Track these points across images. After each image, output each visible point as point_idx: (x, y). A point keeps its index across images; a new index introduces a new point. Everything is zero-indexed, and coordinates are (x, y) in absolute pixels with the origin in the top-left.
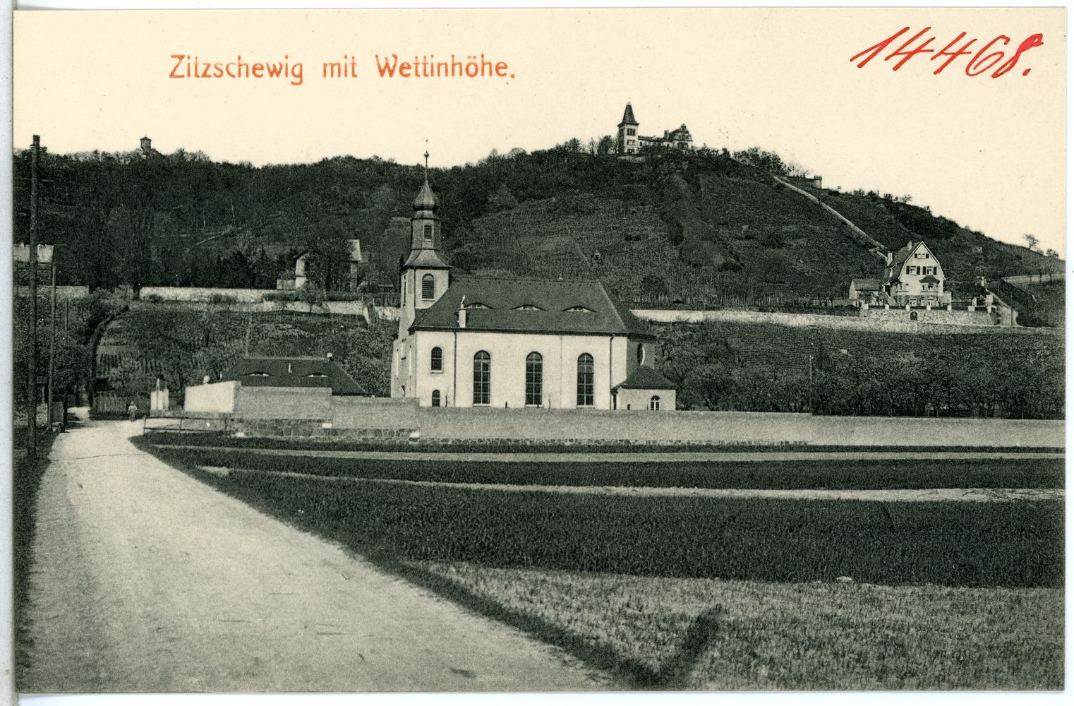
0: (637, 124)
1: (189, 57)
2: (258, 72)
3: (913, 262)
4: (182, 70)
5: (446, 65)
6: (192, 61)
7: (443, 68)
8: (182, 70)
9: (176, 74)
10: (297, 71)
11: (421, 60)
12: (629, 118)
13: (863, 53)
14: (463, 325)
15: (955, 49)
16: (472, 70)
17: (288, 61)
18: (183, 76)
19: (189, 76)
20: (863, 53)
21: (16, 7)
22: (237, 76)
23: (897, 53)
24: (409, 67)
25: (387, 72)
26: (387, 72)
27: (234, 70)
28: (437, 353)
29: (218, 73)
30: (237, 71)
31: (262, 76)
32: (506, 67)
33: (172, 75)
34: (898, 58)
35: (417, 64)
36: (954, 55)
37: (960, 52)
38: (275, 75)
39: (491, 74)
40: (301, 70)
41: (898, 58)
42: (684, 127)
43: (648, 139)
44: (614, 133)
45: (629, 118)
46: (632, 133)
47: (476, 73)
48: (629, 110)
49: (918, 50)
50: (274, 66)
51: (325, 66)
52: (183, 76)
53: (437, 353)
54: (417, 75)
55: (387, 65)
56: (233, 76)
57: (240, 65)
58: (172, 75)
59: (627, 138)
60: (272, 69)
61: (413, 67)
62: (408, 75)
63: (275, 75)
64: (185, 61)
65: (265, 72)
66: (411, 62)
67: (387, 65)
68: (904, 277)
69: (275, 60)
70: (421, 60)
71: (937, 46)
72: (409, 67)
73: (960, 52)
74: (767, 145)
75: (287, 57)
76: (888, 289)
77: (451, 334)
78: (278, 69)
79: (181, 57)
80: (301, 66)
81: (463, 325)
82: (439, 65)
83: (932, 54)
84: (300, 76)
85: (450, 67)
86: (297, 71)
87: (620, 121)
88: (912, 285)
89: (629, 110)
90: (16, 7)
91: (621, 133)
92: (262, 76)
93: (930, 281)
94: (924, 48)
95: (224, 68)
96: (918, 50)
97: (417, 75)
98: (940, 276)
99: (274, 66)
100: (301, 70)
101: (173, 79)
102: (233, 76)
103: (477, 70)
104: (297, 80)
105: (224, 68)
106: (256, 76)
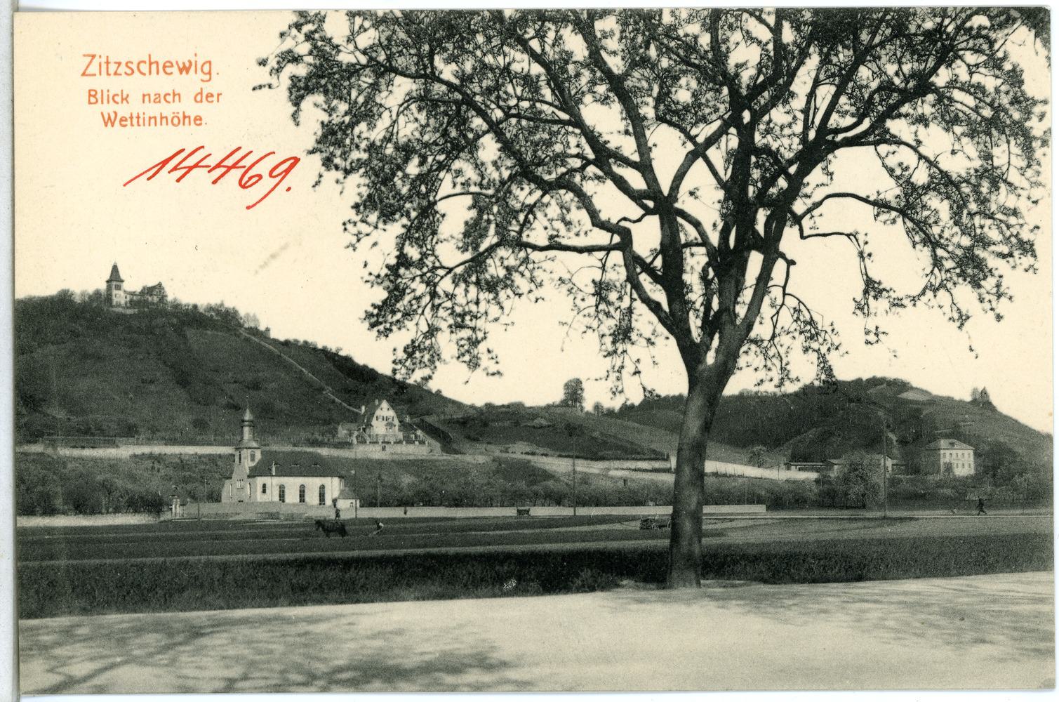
0: (122, 281)
1: (100, 56)
2: (168, 70)
3: (378, 413)
4: (94, 69)
5: (155, 118)
6: (104, 60)
7: (153, 121)
8: (94, 69)
9: (87, 72)
10: (206, 69)
11: (135, 115)
12: (115, 277)
13: (154, 167)
14: (274, 474)
15: (229, 162)
16: (176, 121)
17: (197, 58)
18: (95, 75)
19: (100, 74)
20: (154, 167)
21: (16, 9)
22: (147, 73)
23: (175, 169)
24: (212, 96)
25: (109, 124)
26: (109, 124)
27: (144, 68)
28: (264, 486)
29: (129, 71)
30: (148, 70)
31: (171, 73)
32: (201, 119)
33: (84, 74)
34: (179, 173)
35: (131, 118)
36: (229, 168)
37: (234, 166)
38: (184, 72)
39: (158, 73)
40: (210, 68)
41: (179, 173)
42: (160, 285)
43: (133, 294)
44: (103, 286)
45: (115, 277)
46: (118, 288)
47: (179, 123)
48: (115, 269)
49: (196, 166)
50: (184, 63)
51: (144, 96)
52: (95, 75)
53: (264, 486)
54: (132, 125)
55: (109, 118)
56: (144, 74)
57: (151, 64)
58: (84, 74)
59: (115, 292)
60: (181, 66)
61: (129, 120)
62: (125, 126)
63: (184, 72)
64: (96, 61)
65: (175, 70)
66: (128, 116)
67: (109, 118)
68: (374, 422)
69: (183, 59)
70: (135, 115)
71: (212, 162)
72: (126, 120)
73: (234, 166)
74: (229, 304)
75: (196, 55)
76: (364, 430)
77: (269, 478)
78: (187, 65)
79: (93, 56)
80: (210, 62)
81: (274, 474)
82: (150, 118)
83: (209, 169)
84: (210, 73)
85: (158, 120)
86: (206, 69)
87: (108, 277)
88: (379, 428)
89: (115, 269)
90: (16, 9)
91: (109, 288)
92: (171, 73)
93: (390, 425)
94: (200, 164)
95: (134, 67)
96: (196, 166)
97: (132, 125)
98: (396, 422)
99: (184, 63)
100: (210, 68)
101: (85, 77)
102: (144, 74)
103: (179, 123)
104: (207, 77)
105: (134, 67)
106: (166, 73)
